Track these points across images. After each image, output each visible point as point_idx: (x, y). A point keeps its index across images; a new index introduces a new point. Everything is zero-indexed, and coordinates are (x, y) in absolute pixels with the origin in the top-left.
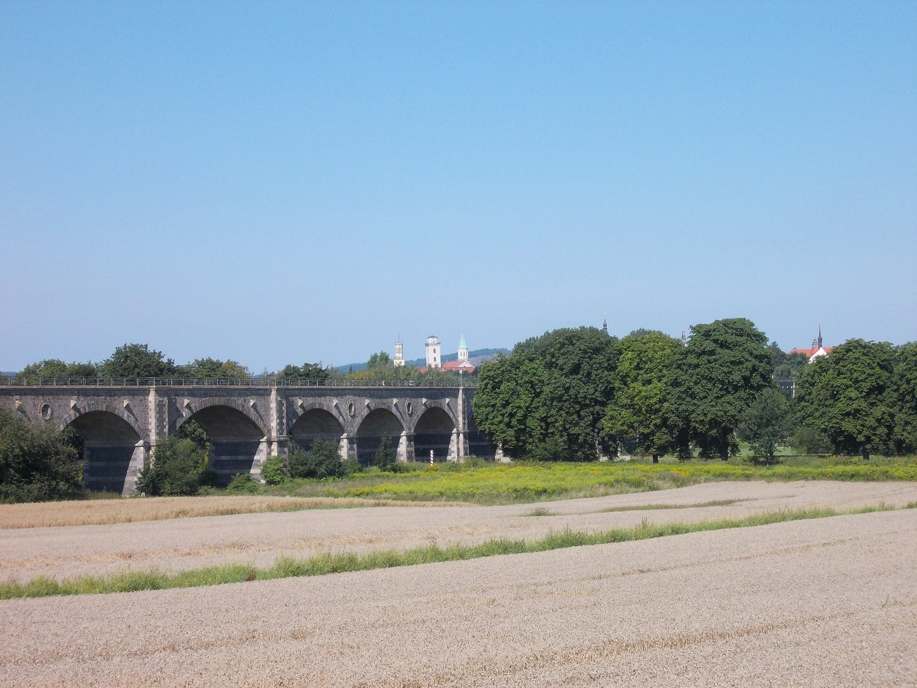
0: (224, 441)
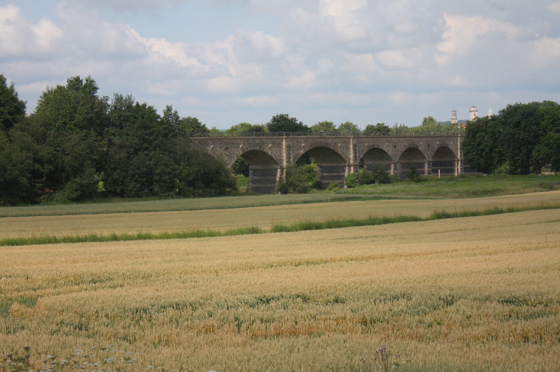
0: (326, 165)
